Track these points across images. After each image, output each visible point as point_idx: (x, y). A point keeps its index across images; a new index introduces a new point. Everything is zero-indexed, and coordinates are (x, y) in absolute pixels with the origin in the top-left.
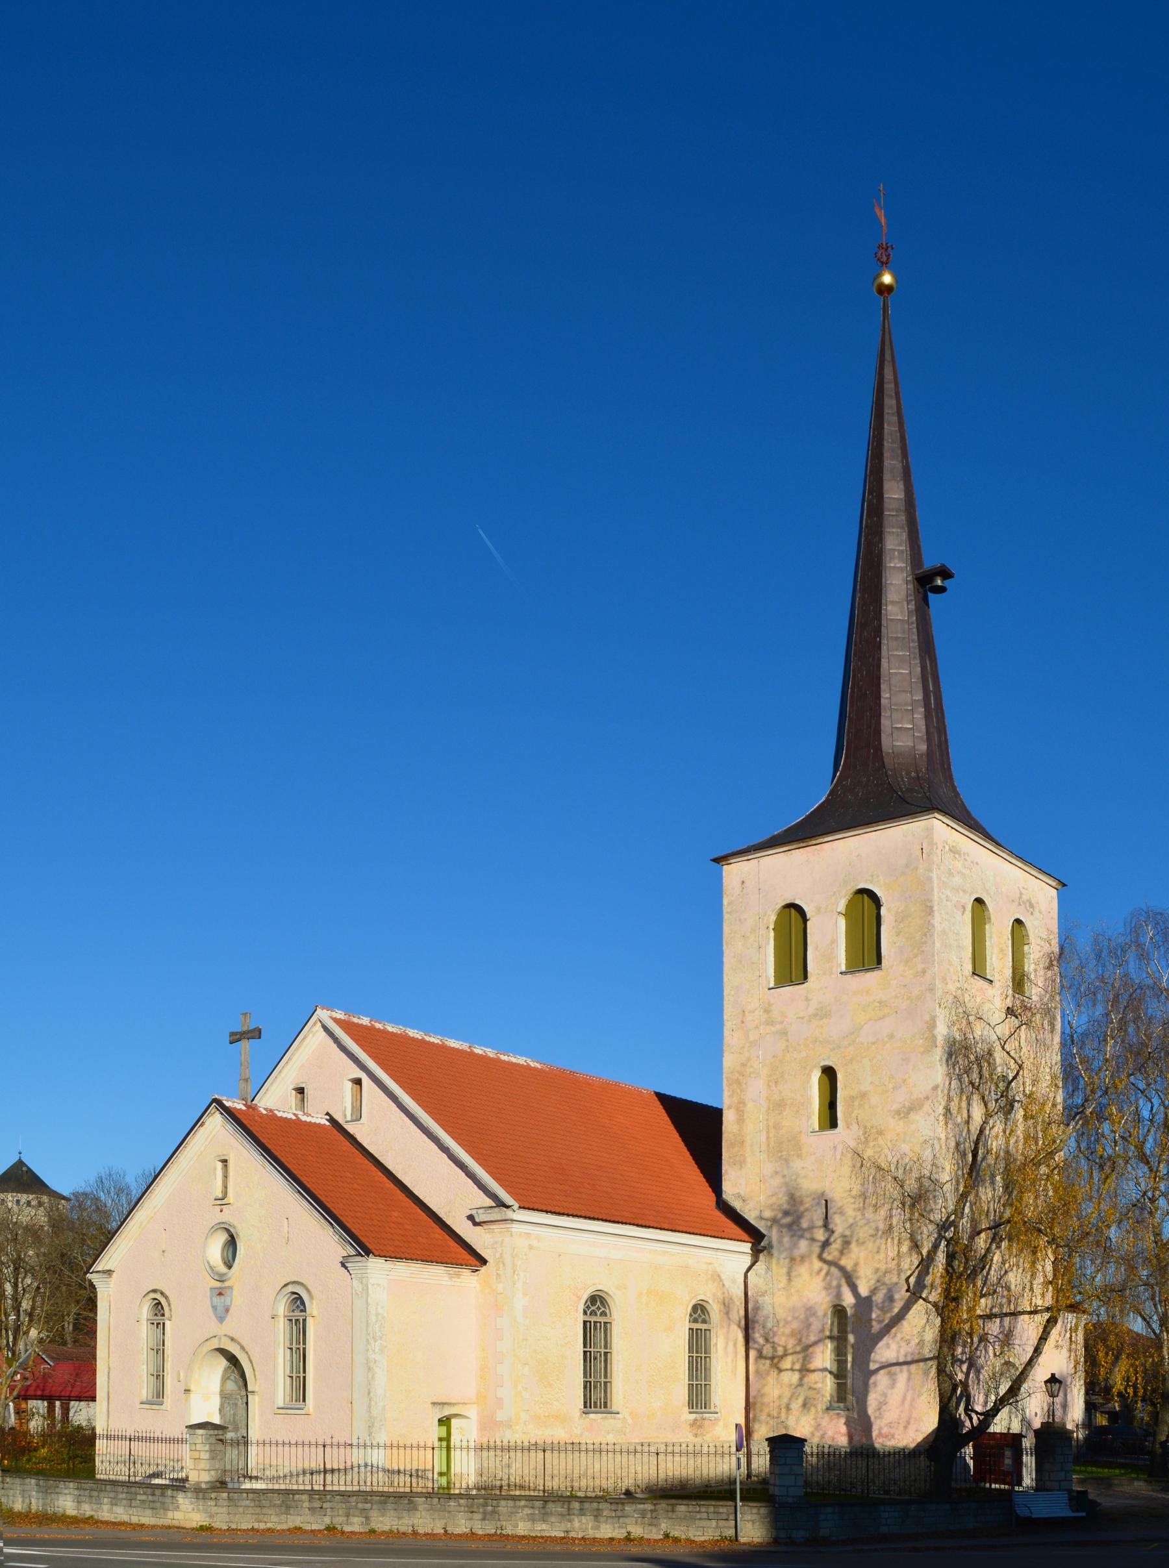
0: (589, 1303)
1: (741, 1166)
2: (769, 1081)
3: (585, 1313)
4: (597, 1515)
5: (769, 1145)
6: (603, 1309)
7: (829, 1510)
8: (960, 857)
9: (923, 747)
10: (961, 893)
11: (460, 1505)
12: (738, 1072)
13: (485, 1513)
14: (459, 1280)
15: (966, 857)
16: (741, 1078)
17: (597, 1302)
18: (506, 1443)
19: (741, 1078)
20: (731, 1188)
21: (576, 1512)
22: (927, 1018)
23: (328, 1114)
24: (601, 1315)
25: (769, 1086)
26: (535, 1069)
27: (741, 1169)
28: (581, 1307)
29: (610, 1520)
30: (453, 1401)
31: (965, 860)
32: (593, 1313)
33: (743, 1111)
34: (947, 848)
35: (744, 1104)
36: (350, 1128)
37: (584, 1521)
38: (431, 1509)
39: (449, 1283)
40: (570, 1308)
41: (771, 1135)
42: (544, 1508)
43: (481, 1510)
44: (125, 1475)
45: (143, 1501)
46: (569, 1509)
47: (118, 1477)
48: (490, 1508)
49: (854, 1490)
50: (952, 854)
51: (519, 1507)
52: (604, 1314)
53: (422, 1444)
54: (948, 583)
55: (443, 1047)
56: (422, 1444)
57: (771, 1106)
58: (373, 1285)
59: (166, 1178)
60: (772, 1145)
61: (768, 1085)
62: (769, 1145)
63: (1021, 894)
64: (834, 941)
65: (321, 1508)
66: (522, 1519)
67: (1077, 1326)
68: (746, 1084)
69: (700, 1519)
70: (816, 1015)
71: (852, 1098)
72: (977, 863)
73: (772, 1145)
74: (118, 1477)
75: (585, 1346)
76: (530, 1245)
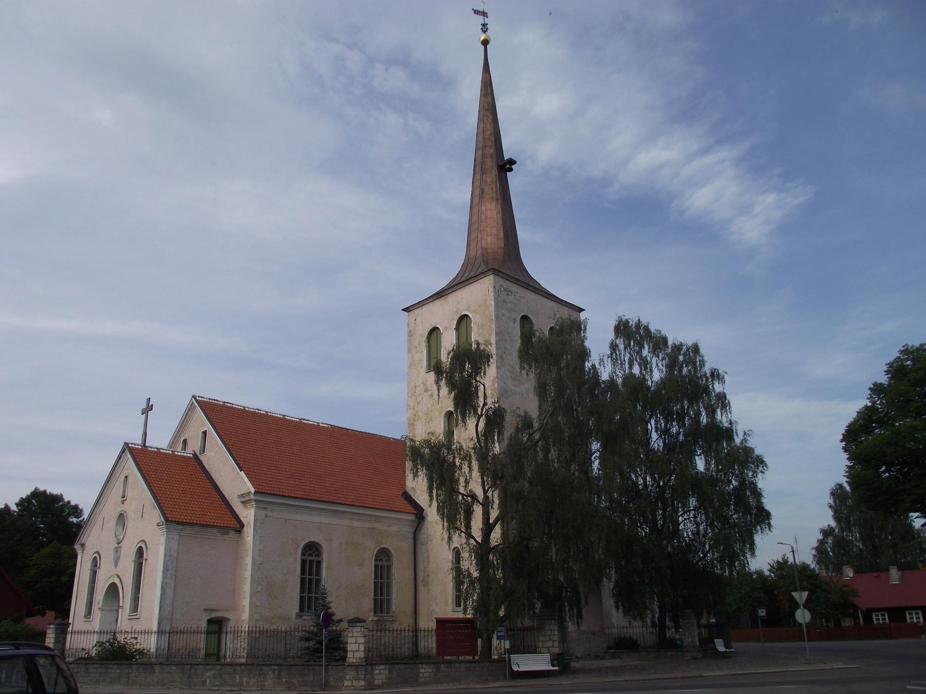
2: (426, 422)
6: (317, 553)
10: (513, 312)
14: (228, 536)
15: (516, 294)
16: (414, 422)
18: (192, 630)
19: (414, 422)
25: (426, 425)
28: (300, 552)
31: (516, 295)
32: (381, 560)
34: (502, 289)
39: (221, 538)
40: (292, 551)
44: (163, 658)
47: (160, 659)
48: (193, 671)
49: (136, 646)
63: (555, 314)
65: (106, 672)
72: (524, 297)
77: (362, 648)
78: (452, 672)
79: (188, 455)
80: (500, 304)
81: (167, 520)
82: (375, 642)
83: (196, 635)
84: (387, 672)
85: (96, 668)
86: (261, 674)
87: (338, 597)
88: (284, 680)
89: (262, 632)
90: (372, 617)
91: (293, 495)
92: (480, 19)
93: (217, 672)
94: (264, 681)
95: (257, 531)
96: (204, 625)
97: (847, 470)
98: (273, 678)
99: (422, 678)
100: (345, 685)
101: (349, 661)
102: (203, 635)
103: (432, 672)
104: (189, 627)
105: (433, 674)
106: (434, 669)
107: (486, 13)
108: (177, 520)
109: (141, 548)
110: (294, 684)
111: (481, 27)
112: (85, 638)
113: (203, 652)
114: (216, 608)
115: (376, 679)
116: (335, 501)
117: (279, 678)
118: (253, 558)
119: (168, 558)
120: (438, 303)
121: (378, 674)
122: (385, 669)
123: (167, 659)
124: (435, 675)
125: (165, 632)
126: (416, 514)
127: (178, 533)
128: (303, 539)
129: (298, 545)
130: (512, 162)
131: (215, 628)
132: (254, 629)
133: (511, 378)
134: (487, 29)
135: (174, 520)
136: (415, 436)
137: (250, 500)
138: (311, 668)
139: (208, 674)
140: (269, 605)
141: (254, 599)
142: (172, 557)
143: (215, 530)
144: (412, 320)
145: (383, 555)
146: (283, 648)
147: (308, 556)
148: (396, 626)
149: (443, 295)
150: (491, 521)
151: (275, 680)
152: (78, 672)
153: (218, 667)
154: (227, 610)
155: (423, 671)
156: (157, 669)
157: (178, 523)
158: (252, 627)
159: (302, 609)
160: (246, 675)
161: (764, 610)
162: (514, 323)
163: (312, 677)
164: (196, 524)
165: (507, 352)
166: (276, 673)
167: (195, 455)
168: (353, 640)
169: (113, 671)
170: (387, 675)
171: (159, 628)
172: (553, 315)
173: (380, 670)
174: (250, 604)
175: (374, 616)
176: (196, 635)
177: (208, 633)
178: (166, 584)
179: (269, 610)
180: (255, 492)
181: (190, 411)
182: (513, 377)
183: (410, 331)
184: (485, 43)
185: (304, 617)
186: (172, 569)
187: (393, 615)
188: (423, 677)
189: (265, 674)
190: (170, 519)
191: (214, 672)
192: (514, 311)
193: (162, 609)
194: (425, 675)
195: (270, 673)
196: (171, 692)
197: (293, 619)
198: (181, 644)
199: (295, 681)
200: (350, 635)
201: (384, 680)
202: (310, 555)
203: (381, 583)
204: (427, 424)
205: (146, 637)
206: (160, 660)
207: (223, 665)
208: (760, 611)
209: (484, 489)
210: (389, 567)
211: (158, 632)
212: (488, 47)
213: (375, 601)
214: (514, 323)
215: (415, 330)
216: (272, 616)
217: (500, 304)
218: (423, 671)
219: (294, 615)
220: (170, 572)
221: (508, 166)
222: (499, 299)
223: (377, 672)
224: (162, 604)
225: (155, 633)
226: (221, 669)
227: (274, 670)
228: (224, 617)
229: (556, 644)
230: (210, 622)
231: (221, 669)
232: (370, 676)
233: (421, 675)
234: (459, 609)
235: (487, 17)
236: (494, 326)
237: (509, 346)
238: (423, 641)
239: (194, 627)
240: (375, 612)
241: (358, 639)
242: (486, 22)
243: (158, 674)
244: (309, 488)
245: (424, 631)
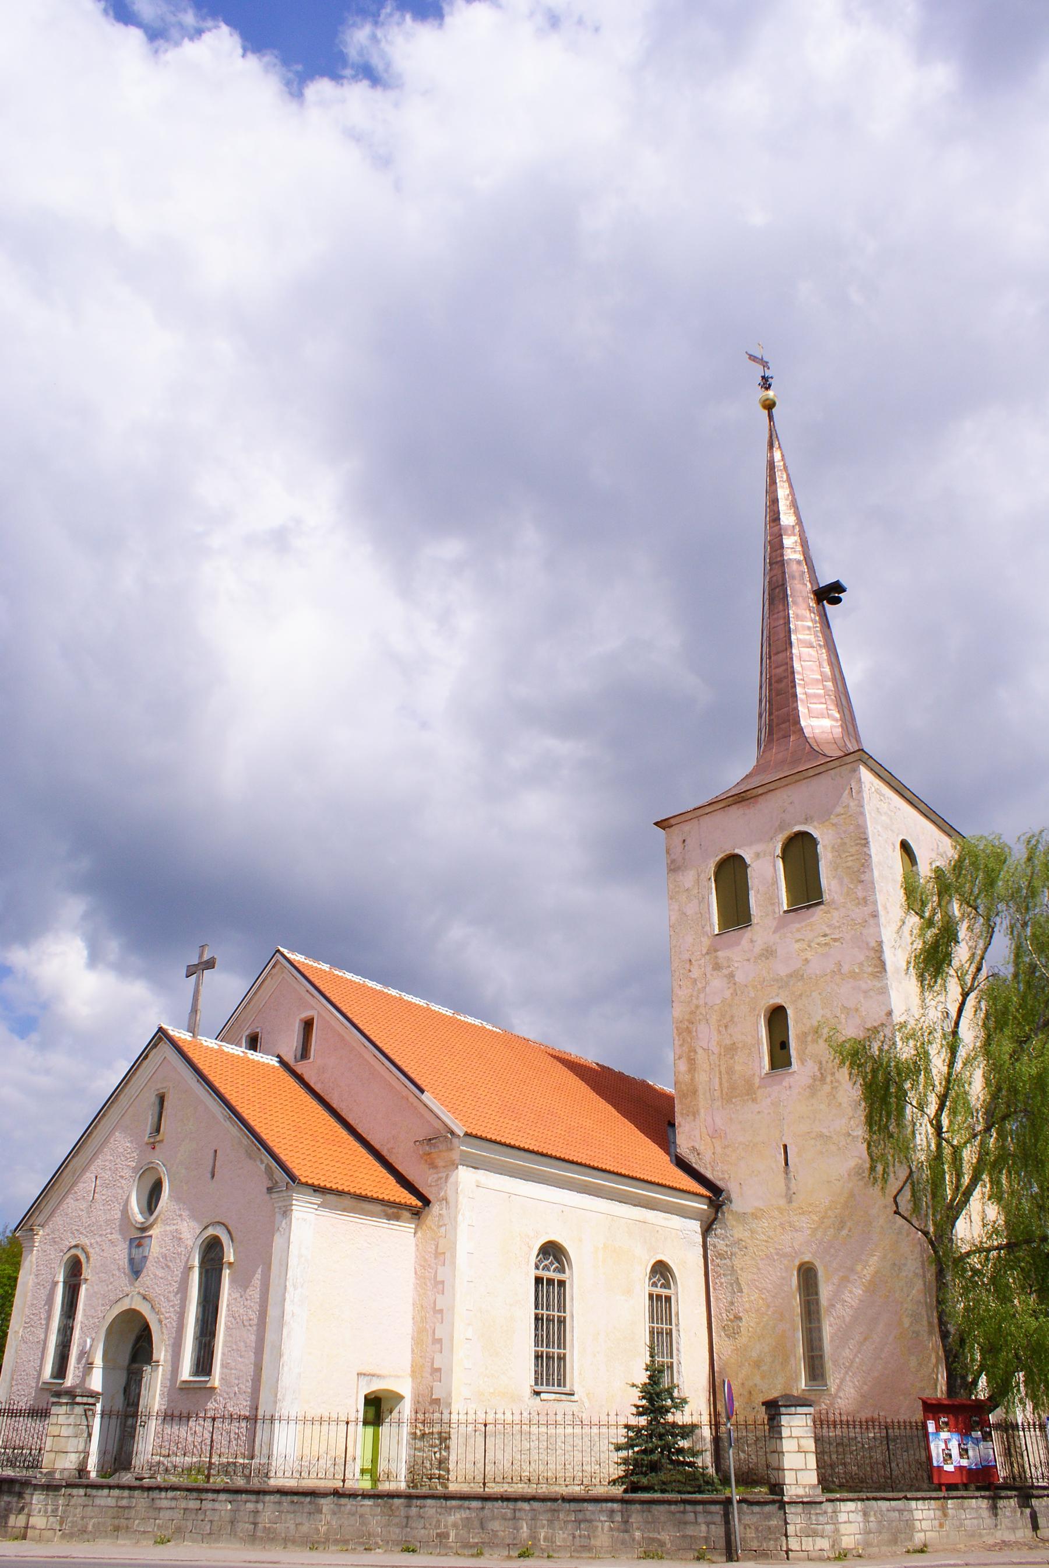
0: (541, 1256)
1: (695, 1117)
2: (719, 1026)
3: (537, 1267)
5: (722, 1091)
12: (688, 1020)
16: (690, 1026)
17: (552, 1252)
20: (684, 1144)
22: (873, 944)
25: (719, 1032)
27: (694, 1120)
28: (533, 1260)
33: (694, 1059)
34: (873, 789)
35: (695, 1052)
41: (724, 1080)
48: (414, 1511)
53: (334, 1416)
56: (334, 1416)
57: (723, 1050)
58: (298, 1219)
59: (286, 1369)
60: (725, 1090)
61: (719, 1030)
62: (722, 1091)
64: (775, 882)
68: (696, 1031)
70: (762, 955)
71: (805, 1034)
73: (725, 1090)
75: (536, 1308)
76: (477, 1181)
78: (966, 1519)
83: (317, 1426)
84: (859, 1518)
85: (174, 1499)
86: (579, 1522)
88: (638, 1534)
92: (759, 371)
93: (474, 1515)
94: (589, 1537)
98: (611, 1529)
99: (919, 1531)
101: (790, 1493)
105: (936, 1523)
106: (937, 1511)
107: (767, 363)
110: (662, 1544)
112: (316, 1435)
114: (378, 1372)
115: (843, 1535)
117: (626, 1531)
120: (735, 812)
121: (845, 1522)
124: (941, 1525)
127: (314, 1211)
132: (500, 1416)
138: (700, 1508)
139: (451, 1519)
140: (486, 1369)
143: (379, 1208)
144: (677, 841)
145: (661, 1271)
147: (543, 1269)
149: (735, 797)
151: (616, 1534)
152: (129, 1507)
160: (545, 1522)
163: (704, 1528)
164: (348, 1193)
166: (618, 1518)
169: (217, 1505)
170: (861, 1525)
176: (317, 1426)
183: (673, 861)
184: (769, 406)
188: (922, 1530)
189: (590, 1521)
191: (465, 1514)
196: (104, 1550)
197: (526, 1399)
198: (315, 1448)
199: (664, 1536)
201: (857, 1536)
202: (546, 1268)
204: (723, 1029)
205: (308, 1432)
215: (684, 859)
216: (492, 1390)
219: (527, 1392)
226: (483, 1508)
227: (612, 1511)
228: (392, 1391)
231: (483, 1508)
232: (832, 1526)
235: (769, 368)
241: (803, 1442)
243: (329, 1517)
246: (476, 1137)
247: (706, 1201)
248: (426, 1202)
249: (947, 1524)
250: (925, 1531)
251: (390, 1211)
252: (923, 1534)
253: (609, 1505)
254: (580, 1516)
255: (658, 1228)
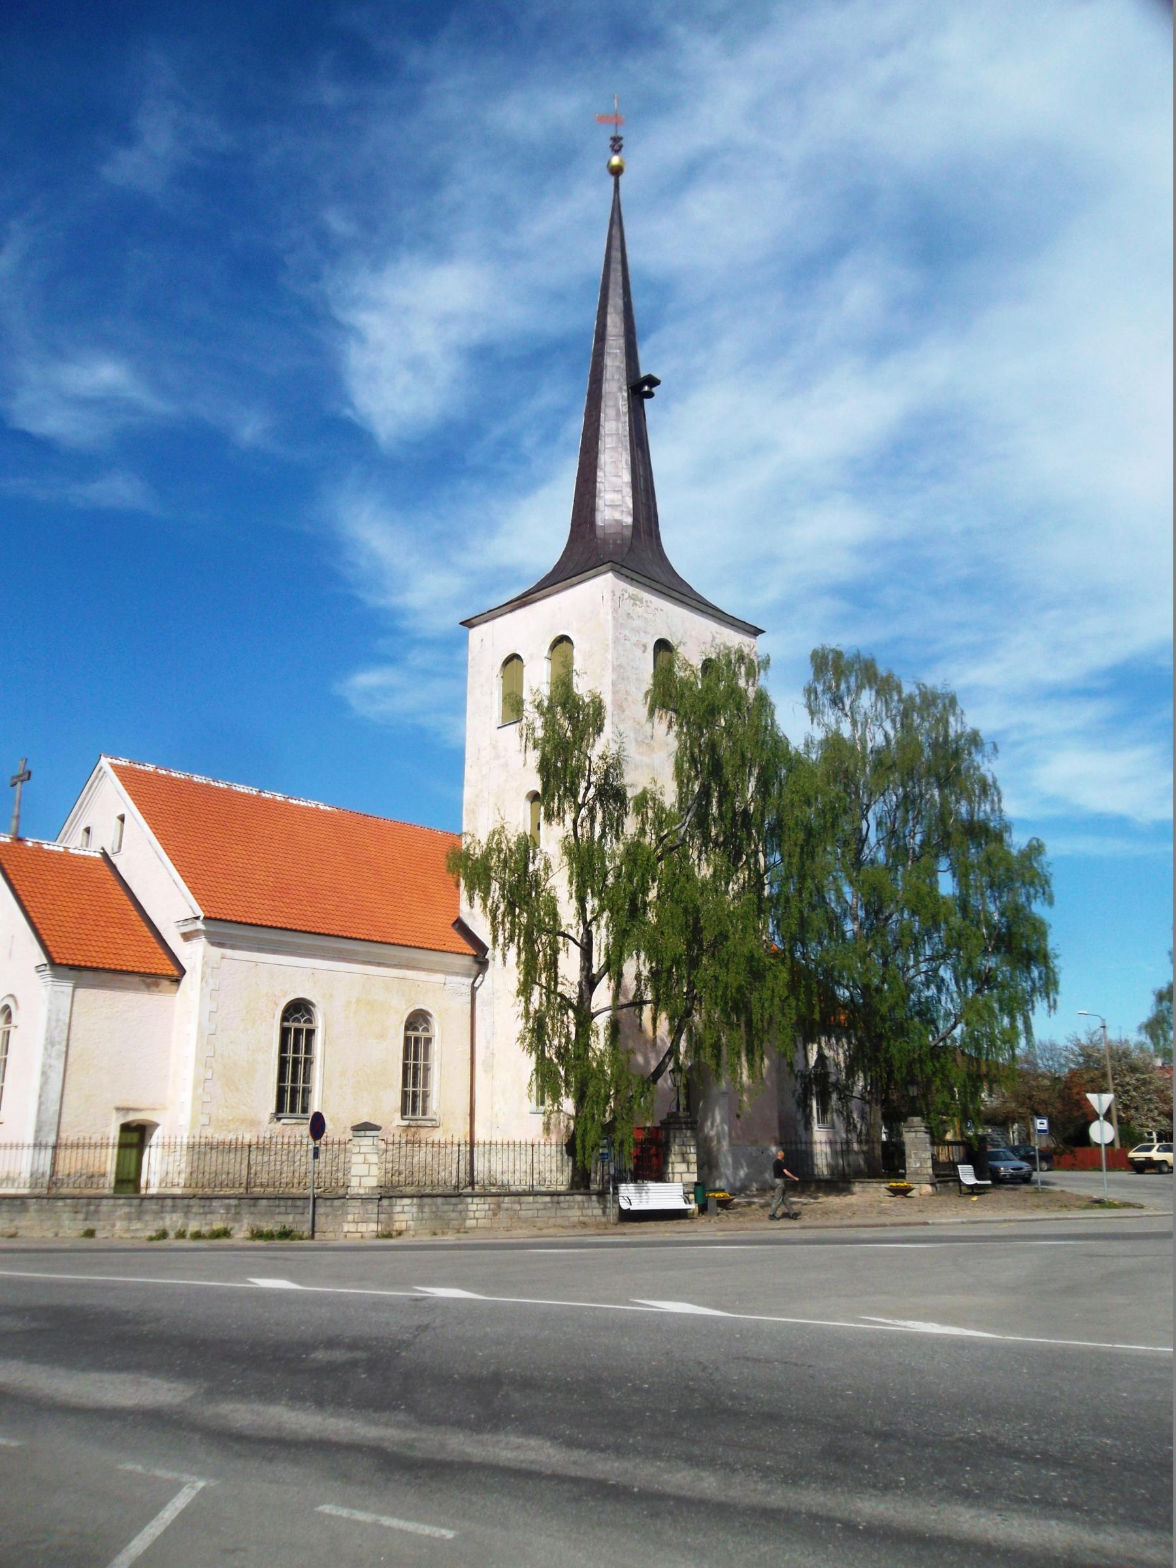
4: (187, 1211)
7: (407, 1201)
8: (642, 602)
9: (629, 520)
10: (642, 634)
11: (65, 1205)
13: (87, 1213)
21: (168, 1209)
23: (103, 849)
24: (423, 1030)
26: (324, 812)
29: (198, 1217)
30: (141, 1106)
31: (648, 606)
36: (114, 859)
37: (174, 1219)
38: (40, 1210)
42: (140, 1205)
43: (84, 1210)
44: (42, 1187)
45: (196, 1214)
46: (162, 1206)
47: (99, 1191)
48: (92, 1208)
50: (632, 601)
51: (119, 1206)
52: (309, 1021)
54: (654, 390)
55: (229, 792)
66: (120, 1218)
67: (987, 1054)
69: (278, 1214)
72: (661, 610)
74: (99, 1191)
77: (375, 1171)
78: (521, 1210)
79: (92, 854)
80: (621, 620)
81: (52, 963)
82: (403, 1160)
84: (414, 1209)
87: (342, 1088)
89: (211, 1146)
90: (398, 1120)
91: (269, 924)
95: (206, 982)
96: (114, 1134)
97: (338, 222)
100: (346, 1229)
102: (110, 1150)
103: (489, 1210)
104: (87, 1137)
105: (490, 1213)
108: (71, 962)
109: (7, 1007)
111: (610, 143)
113: (111, 1178)
116: (340, 934)
118: (200, 1024)
119: (53, 1024)
122: (411, 1205)
123: (49, 1188)
125: (46, 1146)
126: (475, 956)
128: (285, 994)
129: (277, 1005)
130: (653, 381)
131: (134, 1137)
132: (173, 1140)
133: (636, 740)
134: (621, 147)
135: (65, 962)
136: (477, 830)
137: (197, 931)
140: (226, 1100)
141: (200, 1090)
142: (60, 1023)
143: (137, 979)
146: (244, 1173)
148: (437, 1136)
150: (595, 970)
153: (136, 1202)
154: (154, 1109)
155: (474, 1207)
156: (33, 1204)
157: (72, 967)
158: (459, 1145)
159: (280, 1108)
161: (1045, 1121)
162: (644, 652)
165: (630, 698)
167: (105, 855)
168: (360, 1158)
170: (415, 1215)
171: (36, 1138)
172: (710, 638)
173: (403, 1206)
174: (194, 1099)
175: (403, 1119)
177: (122, 1146)
178: (50, 1066)
179: (225, 1110)
180: (205, 918)
181: (97, 781)
182: (639, 739)
184: (616, 172)
185: (283, 1121)
186: (60, 1044)
187: (434, 1117)
190: (58, 961)
192: (646, 633)
193: (43, 1107)
194: (477, 1214)
195: (222, 1211)
200: (356, 1150)
203: (415, 1066)
206: (37, 1191)
207: (143, 1198)
208: (1039, 1121)
209: (585, 922)
210: (428, 1041)
211: (35, 1146)
212: (622, 179)
213: (405, 1094)
214: (644, 652)
216: (230, 1118)
217: (621, 620)
218: (474, 1207)
220: (57, 1047)
221: (646, 388)
222: (620, 611)
223: (398, 1209)
224: (42, 1099)
225: (114, 1146)
229: (694, 1168)
230: (126, 1128)
232: (386, 1216)
233: (471, 1214)
234: (542, 1108)
236: (610, 657)
237: (634, 689)
238: (481, 1159)
239: (96, 1138)
240: (404, 1112)
241: (368, 1156)
242: (620, 134)
244: (296, 912)
245: (484, 1144)
246: (216, 919)
247: (470, 958)
248: (183, 971)
249: (501, 1214)
250: (477, 1219)
251: (149, 980)
252: (475, 1221)
253: (227, 1201)
254: (206, 1209)
255: (419, 983)
